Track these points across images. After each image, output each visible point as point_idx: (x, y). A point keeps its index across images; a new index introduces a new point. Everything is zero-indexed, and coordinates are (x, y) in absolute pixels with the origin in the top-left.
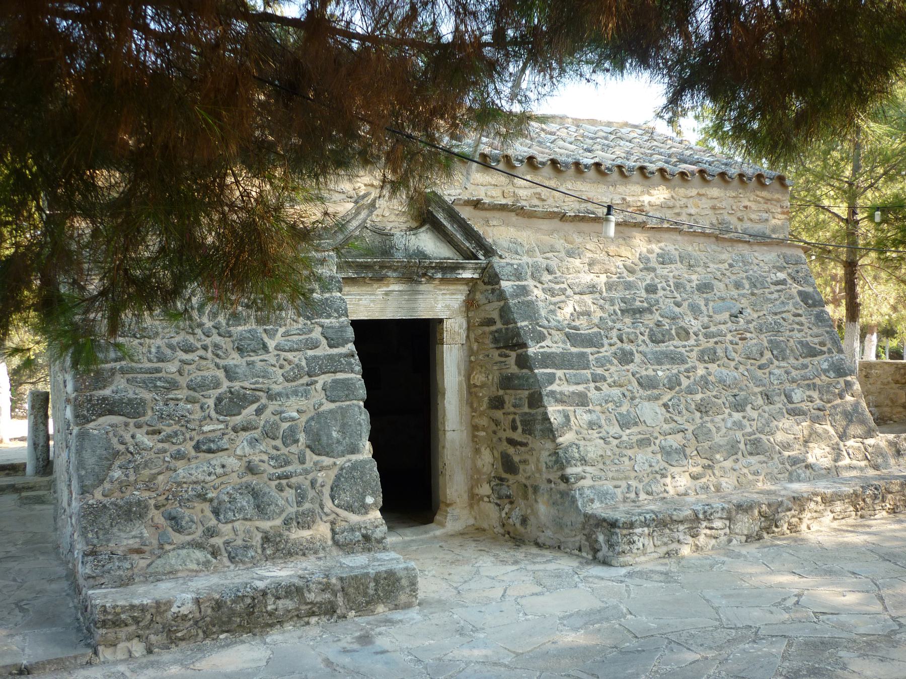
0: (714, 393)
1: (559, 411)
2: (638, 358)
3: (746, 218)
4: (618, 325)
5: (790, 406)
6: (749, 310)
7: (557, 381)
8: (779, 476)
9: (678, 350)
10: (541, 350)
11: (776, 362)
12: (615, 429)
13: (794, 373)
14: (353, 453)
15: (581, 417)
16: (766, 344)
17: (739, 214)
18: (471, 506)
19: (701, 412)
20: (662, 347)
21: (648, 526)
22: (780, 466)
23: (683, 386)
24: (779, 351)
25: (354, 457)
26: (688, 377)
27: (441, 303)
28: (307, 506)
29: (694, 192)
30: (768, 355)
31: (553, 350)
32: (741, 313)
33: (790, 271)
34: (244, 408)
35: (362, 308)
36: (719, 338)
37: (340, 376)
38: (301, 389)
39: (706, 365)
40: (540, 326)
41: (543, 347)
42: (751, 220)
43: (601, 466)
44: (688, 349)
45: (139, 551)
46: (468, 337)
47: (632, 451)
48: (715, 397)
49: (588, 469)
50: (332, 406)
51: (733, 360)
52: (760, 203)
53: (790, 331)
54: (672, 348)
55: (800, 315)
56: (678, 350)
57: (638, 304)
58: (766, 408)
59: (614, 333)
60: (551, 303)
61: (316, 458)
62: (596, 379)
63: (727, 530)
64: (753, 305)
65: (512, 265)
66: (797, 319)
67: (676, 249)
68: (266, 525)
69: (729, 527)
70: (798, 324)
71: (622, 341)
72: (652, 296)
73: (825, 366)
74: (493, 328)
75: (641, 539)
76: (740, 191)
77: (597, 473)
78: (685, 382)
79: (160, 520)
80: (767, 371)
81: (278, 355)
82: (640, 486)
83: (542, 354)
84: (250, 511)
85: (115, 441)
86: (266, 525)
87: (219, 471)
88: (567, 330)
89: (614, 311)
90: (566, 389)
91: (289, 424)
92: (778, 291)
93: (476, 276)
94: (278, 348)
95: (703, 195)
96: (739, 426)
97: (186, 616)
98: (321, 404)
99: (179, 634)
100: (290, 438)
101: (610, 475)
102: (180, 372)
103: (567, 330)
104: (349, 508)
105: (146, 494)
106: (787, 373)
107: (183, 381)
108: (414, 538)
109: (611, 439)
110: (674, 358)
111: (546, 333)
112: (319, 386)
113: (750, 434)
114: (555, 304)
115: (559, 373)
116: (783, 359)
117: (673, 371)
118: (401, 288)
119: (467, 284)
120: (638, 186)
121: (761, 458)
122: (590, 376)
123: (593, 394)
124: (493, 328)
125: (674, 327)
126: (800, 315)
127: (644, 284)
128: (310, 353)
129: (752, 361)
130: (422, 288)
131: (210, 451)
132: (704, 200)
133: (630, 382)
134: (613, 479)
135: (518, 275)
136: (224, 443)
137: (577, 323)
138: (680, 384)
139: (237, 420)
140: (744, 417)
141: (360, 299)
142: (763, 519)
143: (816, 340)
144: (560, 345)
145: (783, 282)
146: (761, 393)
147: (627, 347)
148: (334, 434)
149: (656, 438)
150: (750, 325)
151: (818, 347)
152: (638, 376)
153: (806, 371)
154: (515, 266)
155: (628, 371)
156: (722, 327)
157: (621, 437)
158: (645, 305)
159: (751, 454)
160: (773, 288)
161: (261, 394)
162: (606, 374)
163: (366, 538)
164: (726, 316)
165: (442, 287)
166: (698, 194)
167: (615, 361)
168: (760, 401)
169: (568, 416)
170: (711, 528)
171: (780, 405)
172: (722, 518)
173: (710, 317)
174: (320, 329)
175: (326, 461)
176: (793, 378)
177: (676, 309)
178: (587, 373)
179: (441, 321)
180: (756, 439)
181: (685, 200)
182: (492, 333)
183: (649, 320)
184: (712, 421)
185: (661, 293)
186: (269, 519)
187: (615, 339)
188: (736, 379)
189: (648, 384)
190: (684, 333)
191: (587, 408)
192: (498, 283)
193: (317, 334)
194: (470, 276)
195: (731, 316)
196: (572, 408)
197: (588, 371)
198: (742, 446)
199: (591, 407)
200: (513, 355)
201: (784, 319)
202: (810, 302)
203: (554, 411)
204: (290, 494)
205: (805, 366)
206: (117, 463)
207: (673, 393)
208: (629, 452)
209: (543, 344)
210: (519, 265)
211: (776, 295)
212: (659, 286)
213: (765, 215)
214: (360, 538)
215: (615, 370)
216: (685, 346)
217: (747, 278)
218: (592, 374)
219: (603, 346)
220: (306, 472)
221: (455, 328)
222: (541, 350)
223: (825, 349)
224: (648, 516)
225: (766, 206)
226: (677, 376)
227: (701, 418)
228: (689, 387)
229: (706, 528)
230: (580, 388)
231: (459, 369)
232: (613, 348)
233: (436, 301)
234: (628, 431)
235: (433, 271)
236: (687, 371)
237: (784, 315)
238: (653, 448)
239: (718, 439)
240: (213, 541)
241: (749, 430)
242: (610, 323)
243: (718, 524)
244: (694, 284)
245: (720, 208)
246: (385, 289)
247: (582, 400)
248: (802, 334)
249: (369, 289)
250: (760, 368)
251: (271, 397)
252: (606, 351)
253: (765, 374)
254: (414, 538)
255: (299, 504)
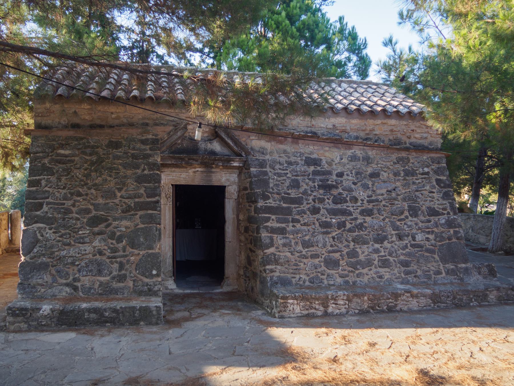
0: (366, 233)
1: (268, 236)
2: (322, 211)
3: (412, 137)
4: (314, 194)
5: (413, 242)
6: (400, 188)
7: (271, 221)
8: (395, 280)
9: (348, 208)
10: (265, 205)
11: (410, 218)
12: (300, 248)
13: (421, 224)
14: (150, 249)
15: (279, 240)
16: (406, 208)
17: (408, 134)
18: (237, 279)
19: (354, 242)
20: (339, 206)
21: (297, 300)
22: (398, 275)
23: (347, 228)
24: (414, 211)
25: (150, 251)
26: (351, 223)
27: (226, 178)
28: (123, 272)
29: (379, 122)
30: (406, 213)
31: (272, 205)
32: (394, 190)
33: (433, 167)
34: (100, 224)
35: (182, 179)
36: (377, 203)
37: (150, 212)
38: (129, 217)
39: (364, 217)
40: (268, 192)
41: (266, 203)
42: (416, 138)
43: (287, 266)
44: (355, 208)
45: (42, 285)
46: (238, 196)
47: (307, 260)
48: (366, 235)
49: (279, 267)
50: (143, 226)
51: (383, 215)
52: (423, 128)
53: (424, 201)
54: (345, 207)
55: (433, 192)
56: (348, 208)
57: (329, 182)
58: (397, 243)
59: (311, 198)
60: (277, 181)
61: (131, 250)
62: (294, 221)
63: (347, 306)
64: (404, 186)
65: (259, 160)
66: (431, 195)
67: (361, 153)
68: (102, 279)
69: (348, 305)
70: (430, 197)
71: (315, 202)
72: (340, 179)
73: (443, 221)
74: (247, 192)
75: (292, 306)
76: (410, 121)
77: (283, 269)
78: (348, 226)
79: (54, 272)
80: (403, 222)
81: (120, 200)
82: (307, 278)
83: (265, 206)
84: (95, 272)
85: (38, 235)
86: (102, 279)
87: (83, 252)
88: (283, 195)
89: (314, 186)
90: (275, 225)
91: (120, 233)
92: (422, 178)
93: (241, 165)
94: (121, 197)
95: (385, 123)
96: (377, 251)
97: (46, 315)
98: (138, 225)
99: (43, 323)
100: (119, 240)
101: (291, 271)
102: (74, 205)
103: (283, 195)
104: (143, 275)
105: (49, 260)
106: (416, 224)
107: (74, 209)
108: (188, 291)
109: (296, 253)
110: (345, 212)
111: (270, 195)
112: (138, 216)
113: (382, 256)
114: (279, 181)
115: (273, 217)
116: (415, 217)
117: (343, 220)
118: (202, 170)
119: (238, 169)
120: (343, 118)
121: (387, 269)
122: (291, 219)
123: (290, 228)
124: (247, 192)
125: (349, 196)
126: (433, 192)
127: (336, 172)
128: (137, 200)
129: (395, 217)
130: (213, 170)
131: (80, 243)
132: (386, 126)
133: (314, 224)
134: (292, 273)
135: (262, 164)
136: (87, 240)
137: (290, 191)
138: (345, 227)
139: (96, 229)
140: (381, 247)
141: (181, 175)
142: (370, 302)
143: (441, 207)
144: (277, 202)
145: (427, 173)
146: (396, 234)
147: (317, 205)
148: (142, 240)
149: (323, 254)
150: (399, 197)
151: (441, 210)
152: (320, 221)
153: (429, 224)
154: (261, 161)
155: (315, 218)
156: (380, 197)
157: (301, 252)
158: (334, 183)
159: (380, 267)
160: (420, 176)
161: (110, 218)
162: (301, 219)
163: (150, 290)
164: (384, 191)
165: (225, 170)
166: (382, 123)
167: (308, 212)
168: (394, 238)
169: (273, 239)
170: (336, 304)
171: (407, 242)
172: (343, 300)
173: (374, 191)
174: (144, 189)
175: (136, 252)
176: (419, 227)
177: (353, 186)
178: (290, 218)
179: (225, 187)
180: (386, 259)
181: (373, 126)
182: (247, 194)
183: (335, 192)
184: (360, 248)
185: (345, 177)
186: (104, 276)
187: (311, 201)
188: (381, 226)
189: (326, 225)
190: (355, 200)
191: (285, 236)
192: (249, 169)
193: (142, 191)
194: (238, 165)
195: (387, 191)
196: (276, 236)
197: (291, 217)
198: (376, 262)
199: (287, 235)
200: (253, 206)
201: (422, 194)
202: (442, 185)
203: (264, 235)
204: (116, 266)
205: (429, 221)
206: (38, 245)
207: (340, 231)
208: (305, 261)
209: (267, 202)
210: (264, 160)
211: (420, 181)
212: (345, 173)
213: (425, 135)
214: (147, 290)
215: (308, 218)
216: (353, 207)
217: (403, 170)
218: (292, 218)
219: (302, 204)
220: (126, 256)
221: (232, 191)
222: (265, 205)
223: (445, 212)
224: (297, 294)
225: (426, 130)
226: (344, 222)
227: (354, 246)
228: (350, 228)
229: (333, 303)
230: (283, 225)
231: (233, 211)
232: (309, 206)
233: (222, 177)
234: (306, 250)
235: (217, 162)
236: (352, 220)
237: (422, 192)
238: (320, 259)
239: (362, 257)
240: (76, 284)
241: (383, 254)
242: (310, 192)
243: (341, 302)
244: (368, 173)
245: (395, 131)
246: (194, 170)
247: (282, 231)
248: (433, 203)
249: (185, 170)
250: (399, 220)
251: (115, 220)
252: (305, 206)
253: (401, 224)
254: (188, 291)
255: (120, 270)
